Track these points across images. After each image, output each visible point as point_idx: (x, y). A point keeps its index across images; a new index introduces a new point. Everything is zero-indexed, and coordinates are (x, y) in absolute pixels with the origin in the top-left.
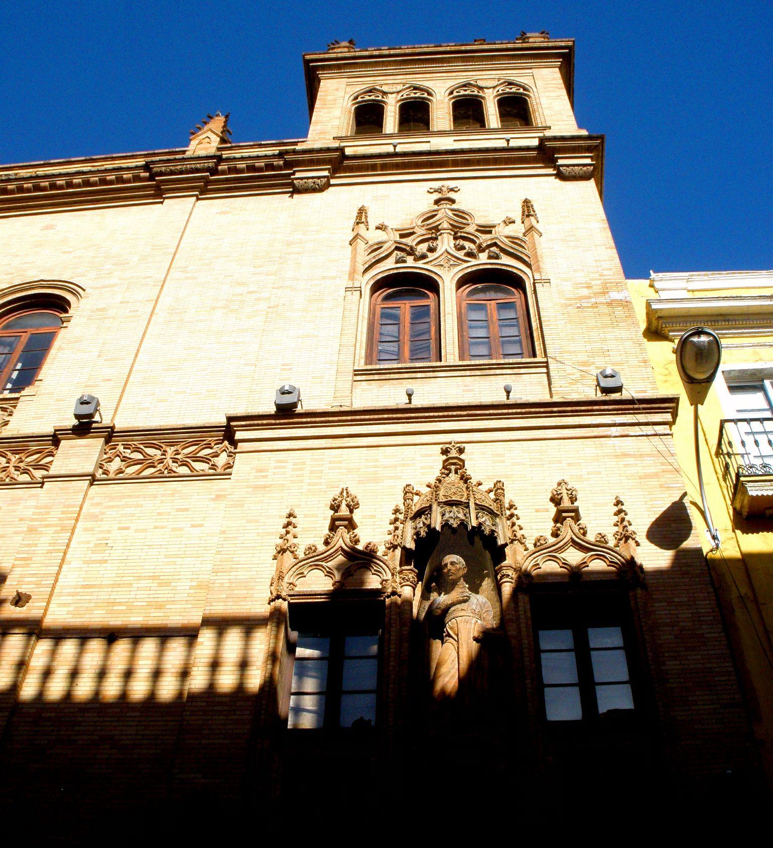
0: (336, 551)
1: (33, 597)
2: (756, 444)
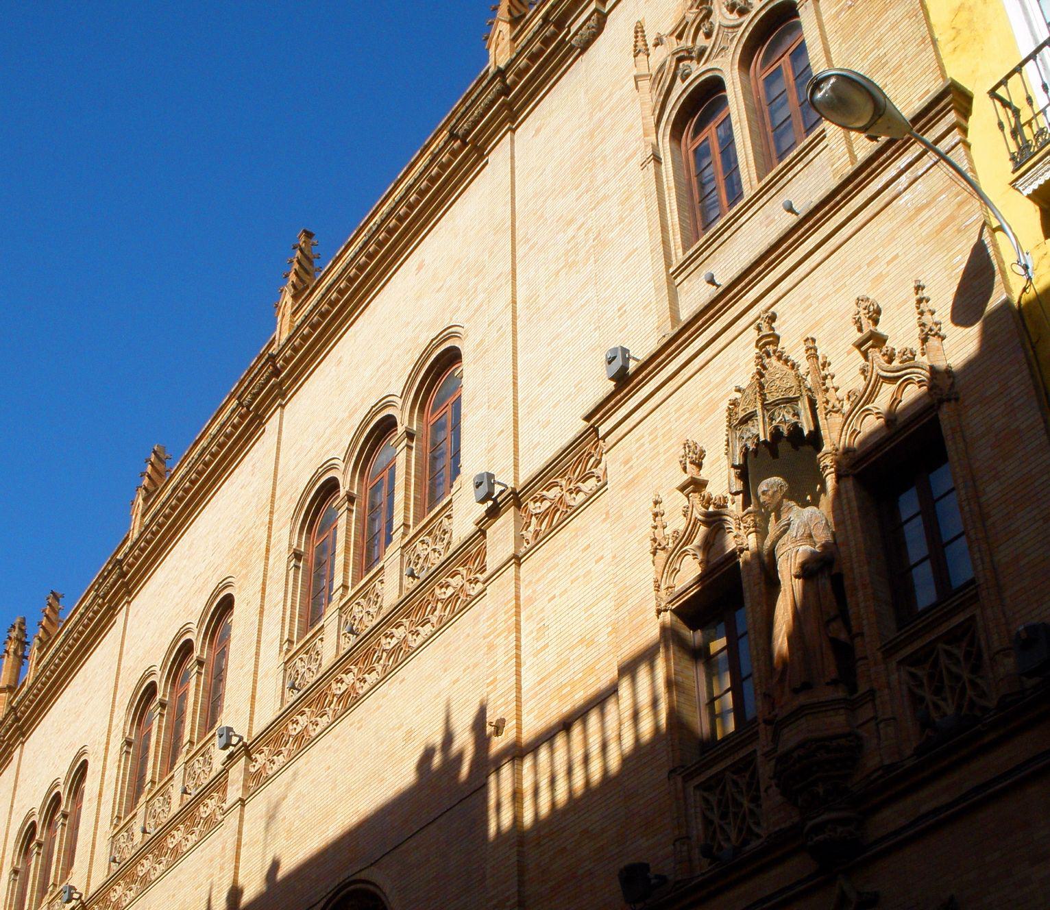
0: (695, 524)
1: (506, 719)
2: (1000, 128)
